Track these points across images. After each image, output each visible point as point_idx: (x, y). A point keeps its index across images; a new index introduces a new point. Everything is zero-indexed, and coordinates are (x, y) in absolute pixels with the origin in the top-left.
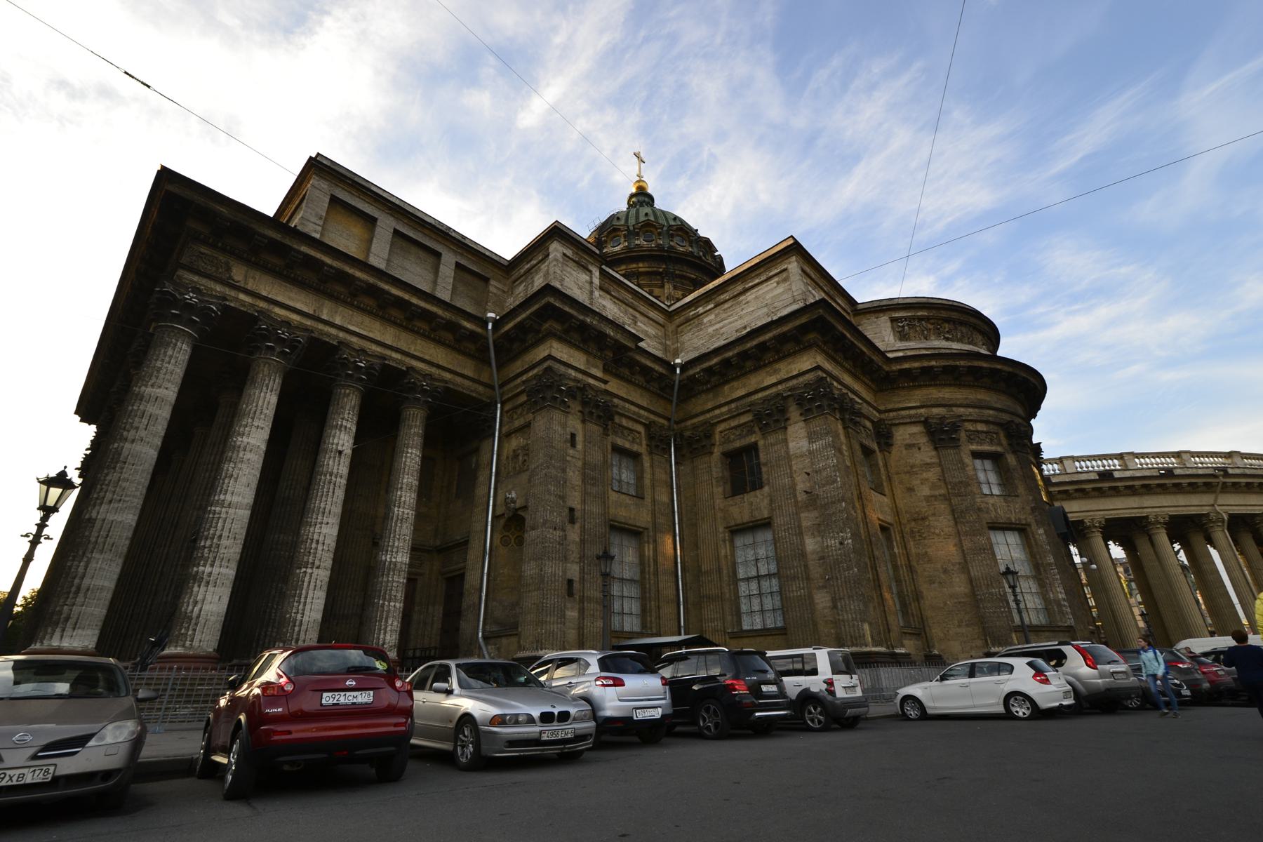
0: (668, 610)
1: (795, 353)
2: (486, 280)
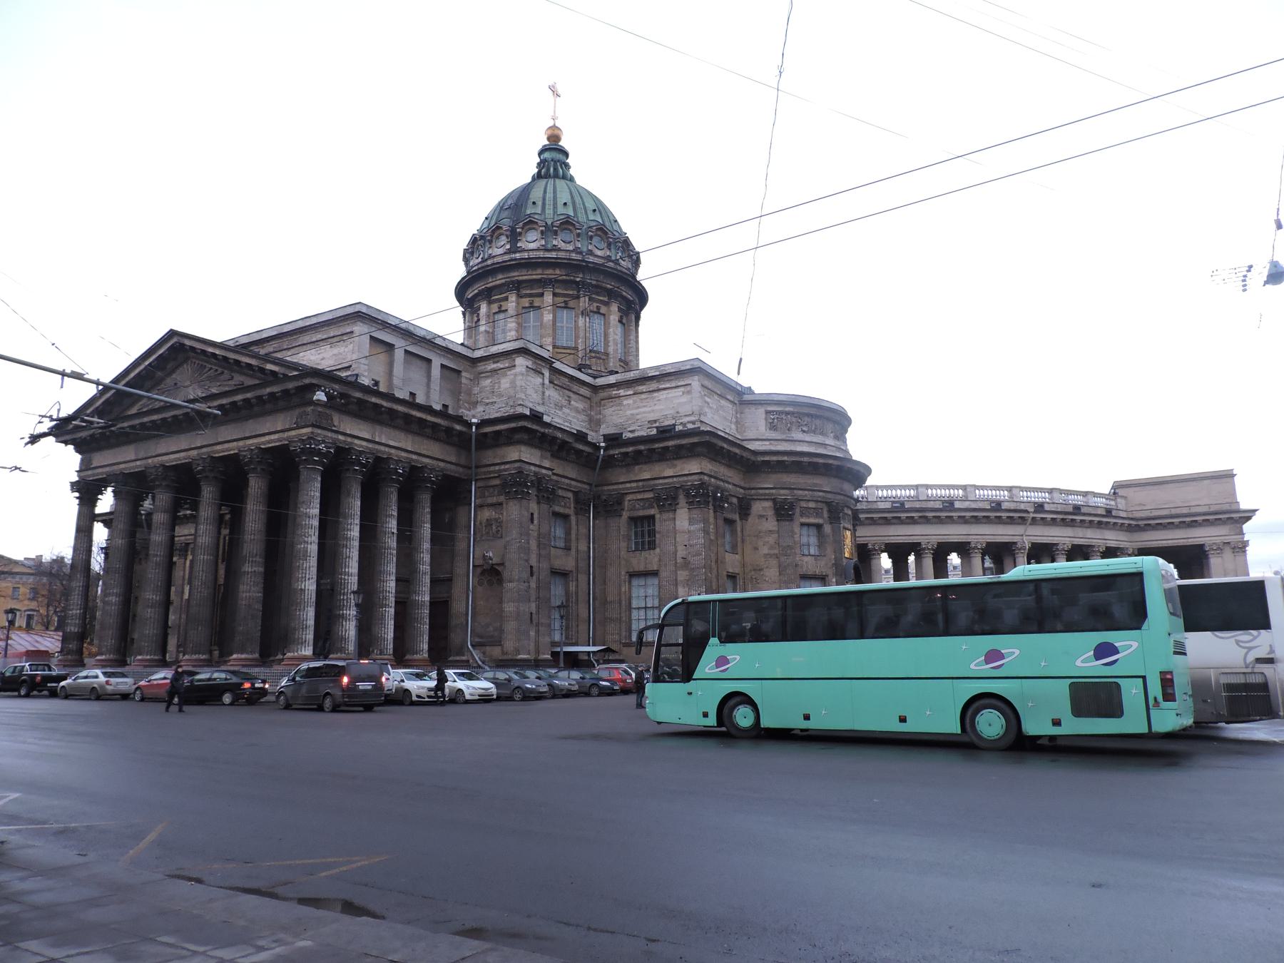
0: (583, 627)
1: (687, 457)
2: (459, 372)
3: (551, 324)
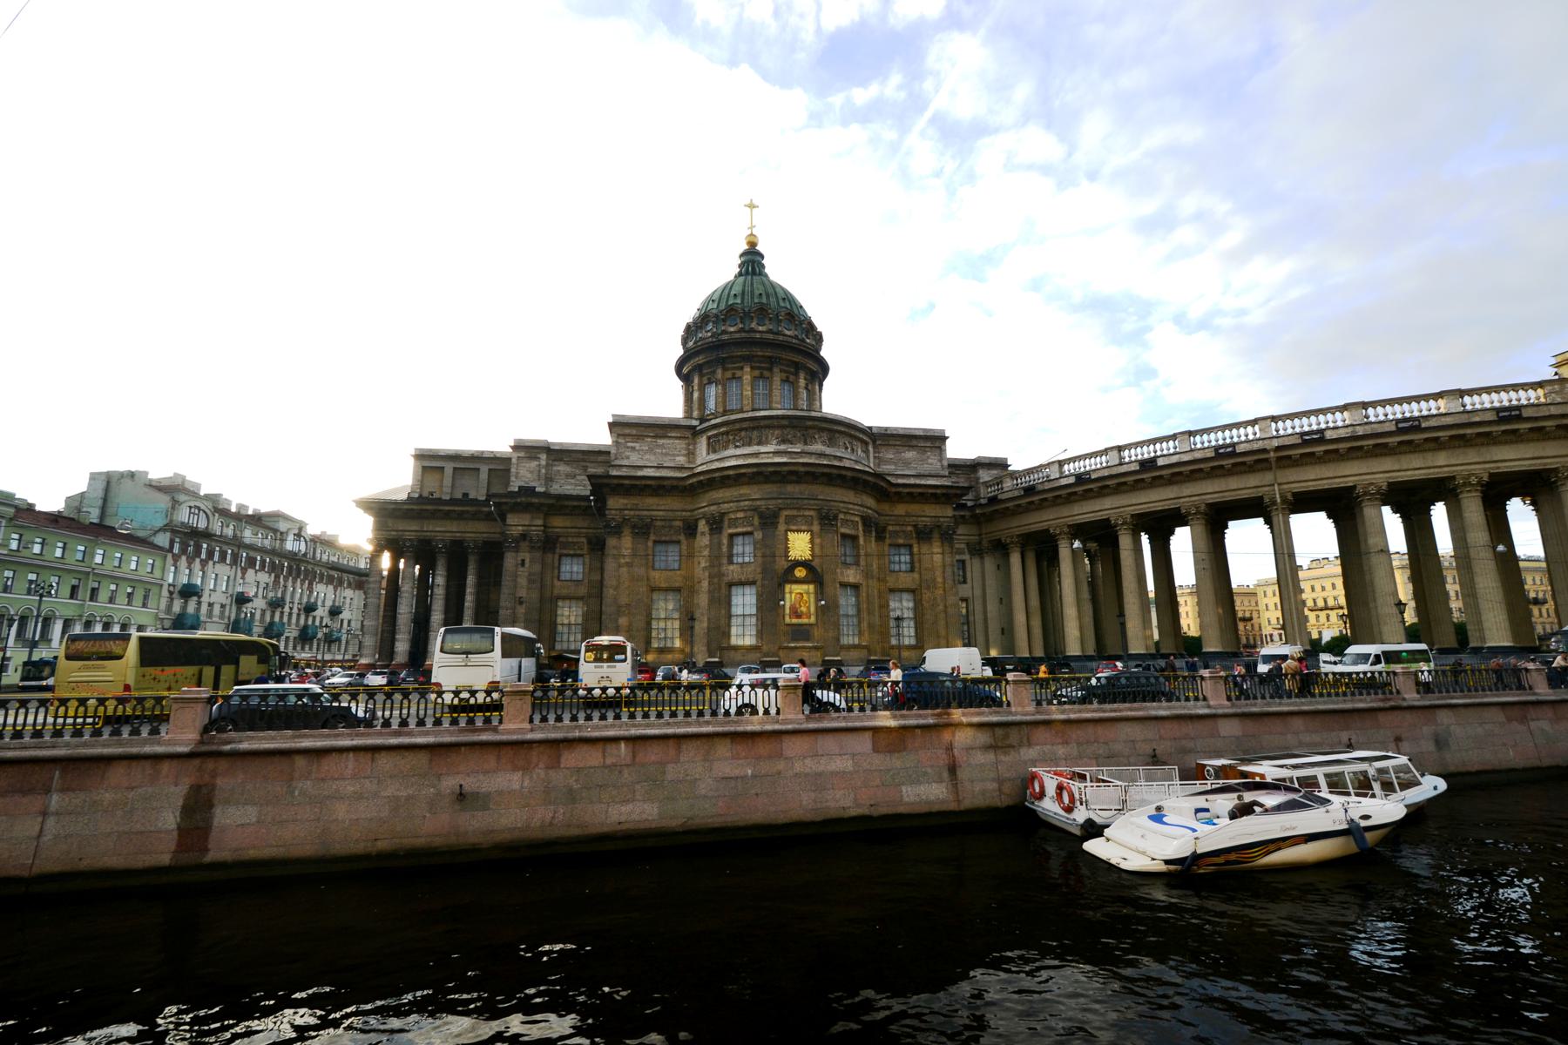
3: (747, 394)
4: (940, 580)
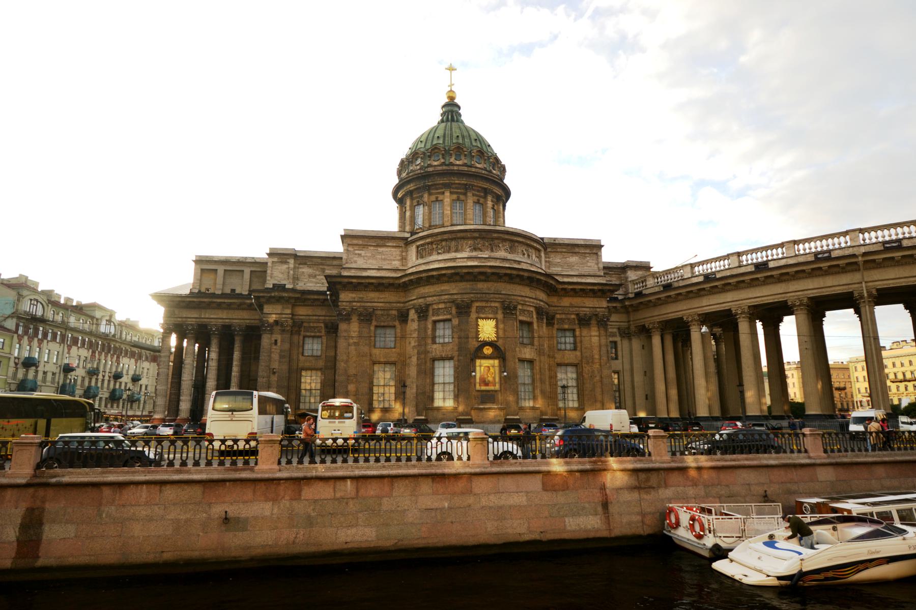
3: (450, 212)
4: (597, 357)
